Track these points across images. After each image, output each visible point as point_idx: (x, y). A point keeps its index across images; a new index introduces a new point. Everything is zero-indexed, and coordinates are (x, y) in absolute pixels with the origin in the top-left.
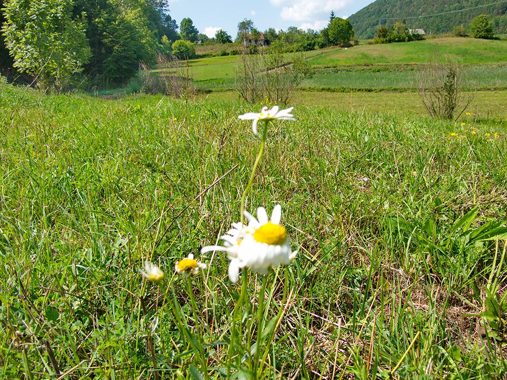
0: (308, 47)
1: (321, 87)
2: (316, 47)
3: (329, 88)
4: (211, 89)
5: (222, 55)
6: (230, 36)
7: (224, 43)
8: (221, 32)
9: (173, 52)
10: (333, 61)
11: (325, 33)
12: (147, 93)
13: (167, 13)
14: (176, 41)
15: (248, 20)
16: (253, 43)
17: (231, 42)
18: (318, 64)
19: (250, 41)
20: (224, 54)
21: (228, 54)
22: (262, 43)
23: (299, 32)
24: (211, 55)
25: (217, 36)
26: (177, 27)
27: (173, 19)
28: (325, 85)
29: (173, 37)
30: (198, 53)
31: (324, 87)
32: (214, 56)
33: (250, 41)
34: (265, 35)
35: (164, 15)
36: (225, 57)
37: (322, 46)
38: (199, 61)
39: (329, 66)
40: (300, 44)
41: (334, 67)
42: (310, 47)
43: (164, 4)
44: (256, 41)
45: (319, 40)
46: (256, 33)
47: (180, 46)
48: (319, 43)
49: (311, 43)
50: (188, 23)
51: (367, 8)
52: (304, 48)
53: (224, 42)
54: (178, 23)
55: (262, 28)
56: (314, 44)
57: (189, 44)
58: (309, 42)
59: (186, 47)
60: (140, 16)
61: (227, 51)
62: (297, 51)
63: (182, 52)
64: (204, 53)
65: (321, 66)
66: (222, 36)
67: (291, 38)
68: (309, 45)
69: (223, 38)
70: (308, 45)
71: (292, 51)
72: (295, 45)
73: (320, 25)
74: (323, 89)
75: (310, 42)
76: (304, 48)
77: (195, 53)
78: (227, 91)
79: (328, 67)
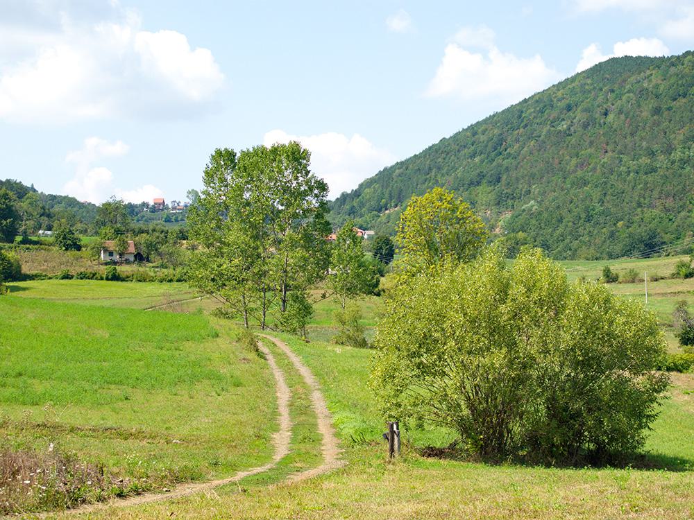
5: (63, 278)
7: (67, 249)
19: (111, 254)
20: (67, 277)
22: (132, 259)
24: (46, 275)
30: (26, 269)
32: (50, 278)
38: (24, 289)
51: (473, 130)
61: (73, 272)
62: (179, 281)
64: (34, 272)
71: (170, 281)
77: (20, 271)
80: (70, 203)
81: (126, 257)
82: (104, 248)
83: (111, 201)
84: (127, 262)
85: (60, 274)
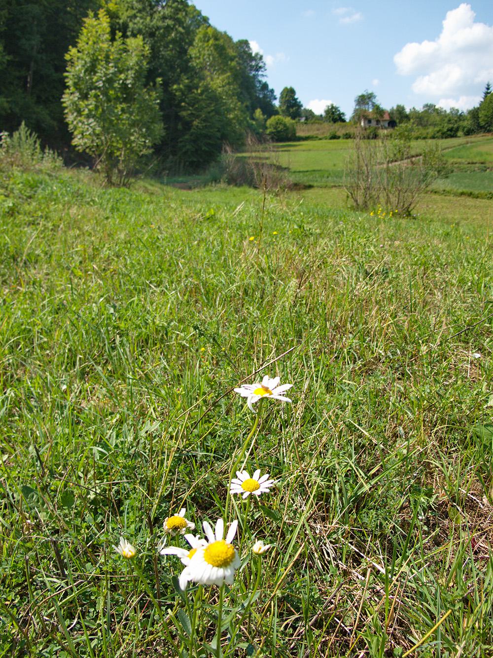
0: (449, 133)
1: (460, 191)
2: (460, 133)
3: (471, 193)
4: (311, 183)
6: (343, 114)
8: (333, 107)
9: (268, 131)
10: (481, 154)
11: (474, 113)
12: (229, 183)
13: (264, 80)
14: (273, 118)
15: (370, 92)
16: (374, 124)
17: (344, 121)
18: (459, 158)
19: (370, 121)
20: (334, 137)
21: (339, 138)
22: (387, 125)
23: (438, 112)
24: (317, 137)
25: (327, 112)
26: (275, 99)
27: (270, 87)
28: (465, 187)
29: (269, 111)
30: (300, 134)
31: (465, 190)
32: (320, 139)
33: (370, 121)
34: (391, 114)
35: (260, 82)
36: (335, 141)
37: (469, 133)
38: (299, 145)
39: (475, 161)
40: (437, 129)
41: (482, 163)
42: (451, 133)
43: (260, 67)
44: (378, 122)
45: (465, 123)
46: (379, 111)
47: (277, 123)
48: (464, 127)
49: (453, 128)
50: (289, 93)
52: (443, 134)
53: (335, 121)
54: (277, 94)
55: (387, 104)
56: (457, 130)
57: (287, 121)
58: (451, 126)
59: (285, 125)
60: (229, 84)
61: (339, 134)
62: (433, 137)
63: (279, 132)
64: (307, 134)
65: (463, 161)
66: (333, 113)
67: (426, 119)
68: (451, 130)
69: (334, 115)
70: (448, 130)
71: (425, 138)
72: (431, 130)
73: (467, 103)
74: (462, 194)
75: (451, 126)
76: (443, 134)
77: (295, 134)
78: (333, 187)
79: (473, 163)
80: (446, 127)
81: (382, 123)
82: (363, 116)
83: (365, 93)
84: (383, 128)
85: (328, 135)
